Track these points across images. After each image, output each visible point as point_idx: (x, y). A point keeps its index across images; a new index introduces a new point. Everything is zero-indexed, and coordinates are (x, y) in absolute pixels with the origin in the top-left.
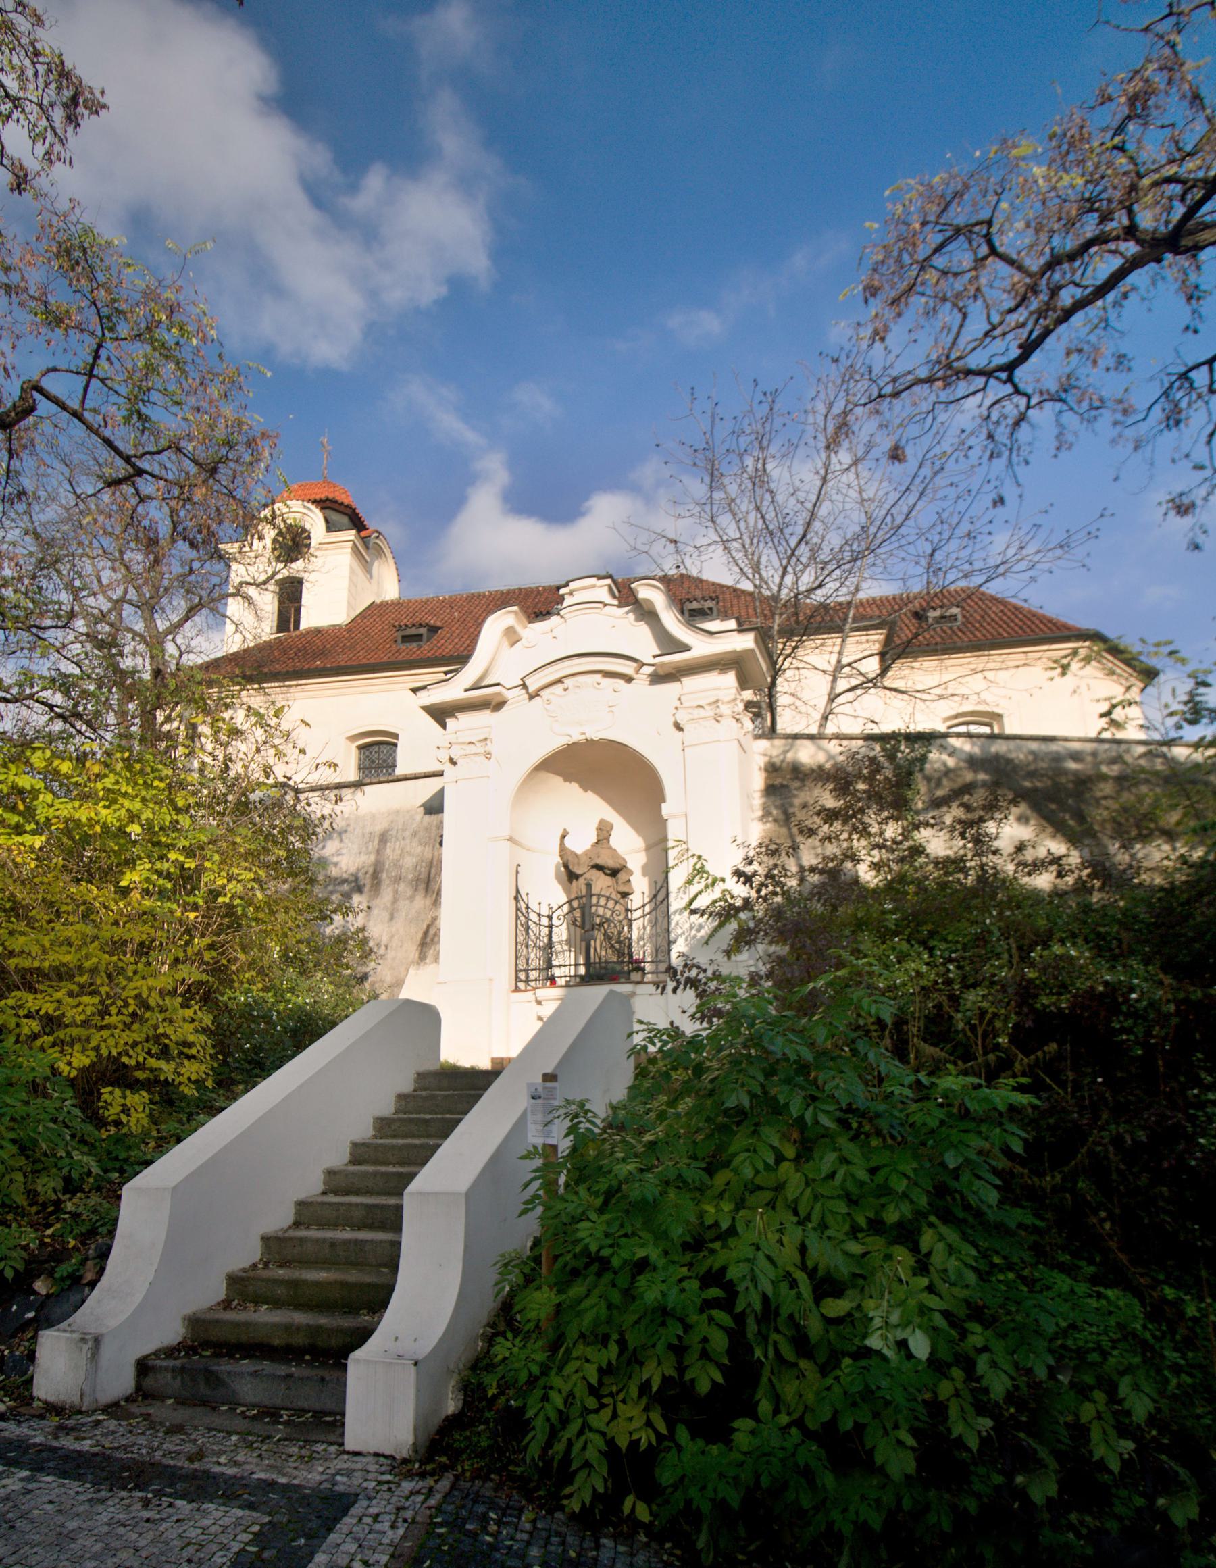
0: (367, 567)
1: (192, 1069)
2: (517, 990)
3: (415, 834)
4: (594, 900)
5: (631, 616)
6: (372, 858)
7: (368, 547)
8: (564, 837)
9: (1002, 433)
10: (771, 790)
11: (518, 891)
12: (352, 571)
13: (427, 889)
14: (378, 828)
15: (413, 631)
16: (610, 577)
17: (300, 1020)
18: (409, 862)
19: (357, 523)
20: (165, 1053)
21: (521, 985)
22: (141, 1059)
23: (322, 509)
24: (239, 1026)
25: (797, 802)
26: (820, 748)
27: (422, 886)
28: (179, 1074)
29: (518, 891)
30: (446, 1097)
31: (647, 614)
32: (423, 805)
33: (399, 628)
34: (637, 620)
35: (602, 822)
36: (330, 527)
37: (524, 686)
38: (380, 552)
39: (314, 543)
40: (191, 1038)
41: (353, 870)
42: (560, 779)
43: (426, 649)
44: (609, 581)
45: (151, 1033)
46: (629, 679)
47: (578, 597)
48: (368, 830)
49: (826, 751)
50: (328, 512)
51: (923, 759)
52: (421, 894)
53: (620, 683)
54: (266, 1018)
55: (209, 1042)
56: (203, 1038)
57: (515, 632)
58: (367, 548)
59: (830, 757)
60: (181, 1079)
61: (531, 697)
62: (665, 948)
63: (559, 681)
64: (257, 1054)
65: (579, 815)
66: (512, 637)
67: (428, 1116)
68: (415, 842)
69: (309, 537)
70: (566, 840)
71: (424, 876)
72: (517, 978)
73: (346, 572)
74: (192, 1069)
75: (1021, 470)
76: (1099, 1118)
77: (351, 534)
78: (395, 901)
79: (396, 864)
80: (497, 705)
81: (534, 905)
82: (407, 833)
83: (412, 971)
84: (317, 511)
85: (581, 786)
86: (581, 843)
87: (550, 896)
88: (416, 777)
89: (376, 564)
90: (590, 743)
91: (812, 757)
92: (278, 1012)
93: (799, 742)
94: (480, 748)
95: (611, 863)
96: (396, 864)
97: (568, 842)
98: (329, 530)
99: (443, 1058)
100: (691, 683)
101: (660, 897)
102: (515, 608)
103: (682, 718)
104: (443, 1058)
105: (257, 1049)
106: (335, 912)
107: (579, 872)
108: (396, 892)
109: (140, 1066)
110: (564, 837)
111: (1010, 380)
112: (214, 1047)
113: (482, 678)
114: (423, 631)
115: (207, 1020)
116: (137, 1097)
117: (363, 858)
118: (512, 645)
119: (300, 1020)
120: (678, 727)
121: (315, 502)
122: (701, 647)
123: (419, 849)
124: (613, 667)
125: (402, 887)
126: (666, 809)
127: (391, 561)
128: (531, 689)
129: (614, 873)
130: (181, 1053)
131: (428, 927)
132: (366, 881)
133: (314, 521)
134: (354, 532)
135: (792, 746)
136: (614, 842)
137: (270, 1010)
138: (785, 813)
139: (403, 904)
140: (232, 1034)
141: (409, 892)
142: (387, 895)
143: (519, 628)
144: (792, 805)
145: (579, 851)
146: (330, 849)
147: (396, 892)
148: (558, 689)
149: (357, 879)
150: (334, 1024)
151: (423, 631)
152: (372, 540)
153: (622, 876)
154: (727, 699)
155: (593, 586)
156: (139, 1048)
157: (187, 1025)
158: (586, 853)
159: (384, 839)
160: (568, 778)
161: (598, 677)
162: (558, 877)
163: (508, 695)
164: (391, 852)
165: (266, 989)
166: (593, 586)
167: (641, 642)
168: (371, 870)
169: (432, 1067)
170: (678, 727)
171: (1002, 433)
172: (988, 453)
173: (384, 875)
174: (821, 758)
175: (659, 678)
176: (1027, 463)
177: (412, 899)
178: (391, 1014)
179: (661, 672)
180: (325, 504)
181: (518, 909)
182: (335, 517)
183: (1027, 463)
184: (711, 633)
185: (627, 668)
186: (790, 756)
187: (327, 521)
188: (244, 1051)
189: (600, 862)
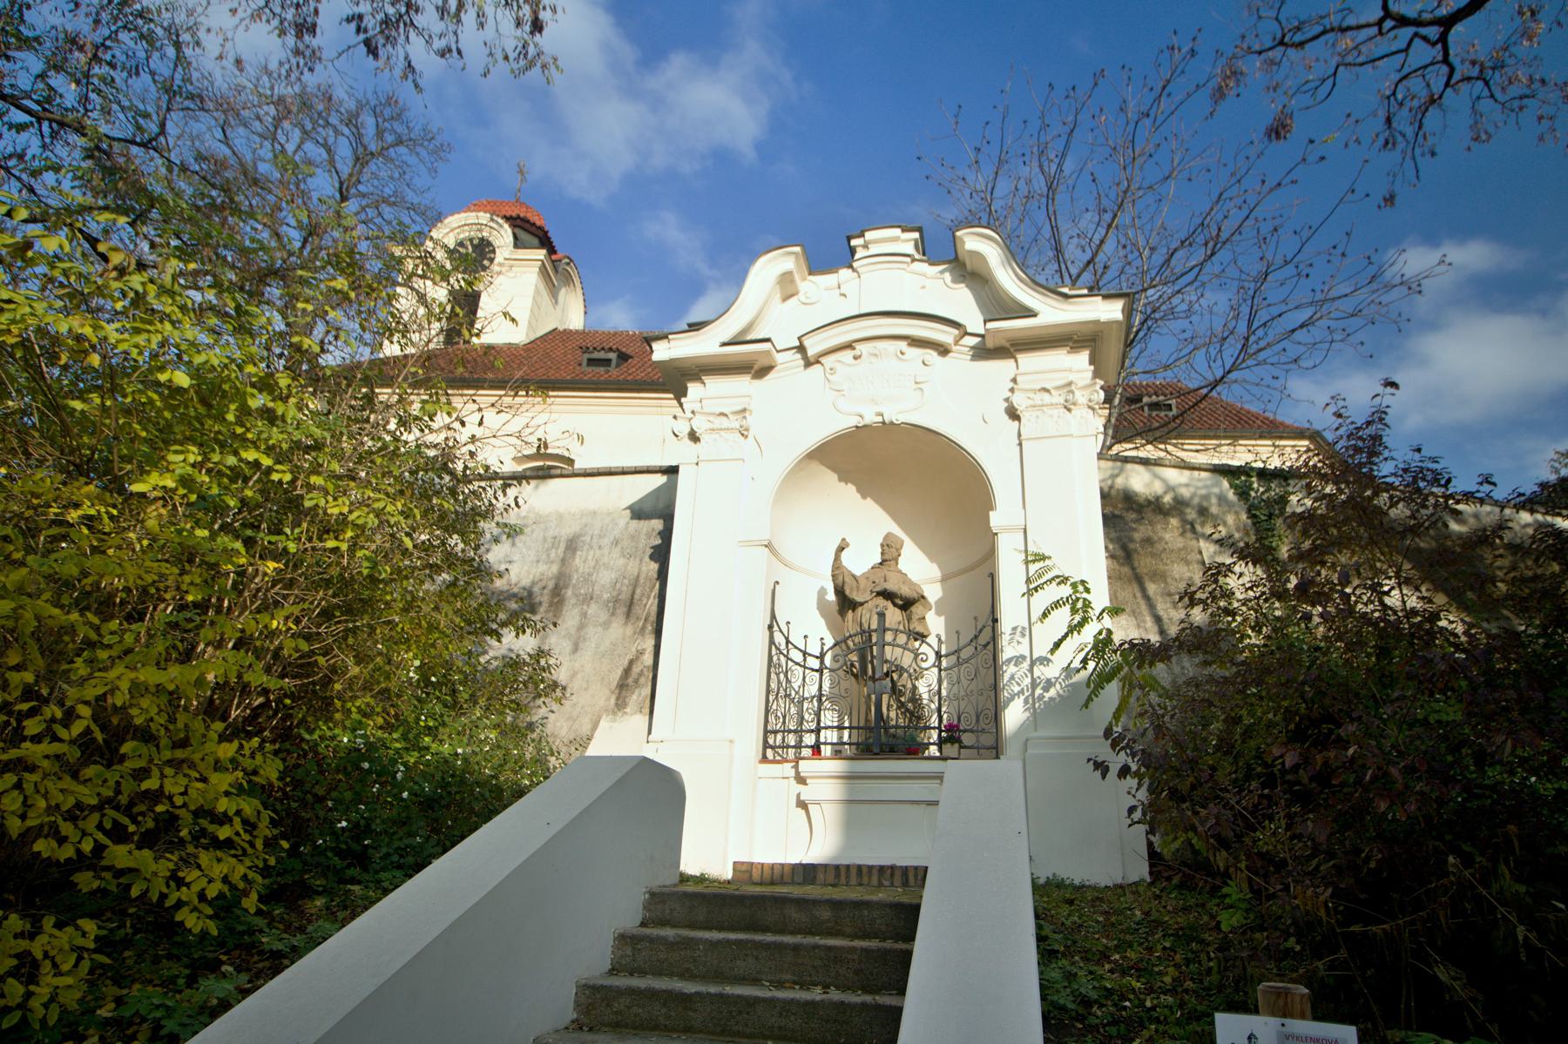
0: (554, 292)
1: (213, 872)
2: (764, 759)
3: (616, 542)
4: (889, 637)
5: (947, 276)
6: (555, 569)
7: (556, 273)
8: (841, 549)
9: (1403, 122)
10: (1109, 520)
11: (773, 617)
12: (537, 292)
13: (628, 614)
14: (567, 531)
15: (602, 355)
16: (919, 230)
17: (444, 785)
18: (605, 577)
19: (545, 242)
20: (161, 836)
21: (770, 753)
22: (87, 846)
23: (513, 226)
24: (333, 787)
25: (1137, 536)
26: (1156, 476)
27: (622, 610)
28: (180, 883)
29: (773, 617)
30: (714, 944)
31: (970, 273)
32: (630, 508)
33: (586, 350)
34: (954, 281)
35: (888, 536)
36: (518, 243)
37: (801, 349)
38: (568, 280)
39: (499, 258)
40: (223, 805)
41: (526, 582)
42: (835, 477)
43: (614, 372)
44: (916, 235)
45: (128, 787)
46: (943, 350)
47: (874, 250)
48: (551, 533)
49: (1164, 480)
50: (517, 231)
51: (1283, 500)
52: (620, 619)
53: (931, 355)
54: (385, 774)
55: (267, 814)
56: (249, 806)
57: (792, 281)
58: (556, 271)
59: (1170, 488)
60: (184, 893)
61: (808, 363)
62: (991, 714)
63: (849, 346)
64: (358, 838)
65: (857, 529)
66: (786, 280)
67: (690, 987)
68: (616, 552)
69: (494, 251)
70: (844, 555)
71: (625, 596)
72: (766, 745)
73: (531, 291)
74: (213, 872)
75: (1425, 163)
76: (1153, 934)
77: (541, 254)
78: (581, 627)
79: (587, 579)
80: (762, 371)
81: (797, 639)
82: (606, 541)
83: (604, 724)
84: (506, 226)
85: (859, 490)
86: (861, 561)
87: (812, 631)
88: (624, 472)
89: (563, 291)
90: (887, 427)
91: (1147, 485)
92: (405, 764)
93: (1129, 466)
94: (734, 423)
95: (905, 591)
96: (587, 579)
97: (846, 557)
98: (516, 246)
99: (691, 863)
100: (1028, 361)
101: (983, 639)
102: (797, 249)
103: (1019, 401)
104: (683, 868)
105: (360, 830)
106: (504, 624)
107: (859, 599)
108: (584, 615)
109: (93, 860)
110: (841, 549)
111: (1443, 39)
112: (273, 823)
113: (745, 331)
114: (612, 356)
115: (271, 771)
116: (66, 936)
117: (542, 568)
118: (786, 298)
119: (444, 785)
120: (1013, 414)
121: (508, 219)
122: (1051, 313)
123: (622, 561)
124: (924, 335)
125: (593, 609)
126: (996, 519)
127: (580, 292)
128: (811, 352)
129: (906, 604)
130: (199, 836)
131: (631, 662)
132: (544, 599)
133: (503, 237)
134: (544, 252)
135: (1122, 470)
136: (903, 564)
137: (394, 762)
138: (1124, 548)
139: (593, 633)
140: (321, 800)
141: (604, 616)
142: (570, 618)
143: (797, 277)
144: (1132, 540)
145: (858, 573)
146: (495, 556)
147: (584, 615)
148: (847, 356)
149: (530, 594)
150: (520, 793)
151: (612, 356)
152: (562, 266)
153: (917, 610)
154: (1081, 384)
155: (896, 239)
156: (91, 823)
157: (220, 777)
158: (866, 576)
159: (572, 546)
160: (844, 477)
161: (903, 345)
162: (822, 605)
163: (779, 358)
164: (581, 563)
165: (387, 727)
166: (896, 239)
167: (961, 304)
168: (551, 585)
169: (666, 880)
170: (1013, 414)
171: (1403, 122)
172: (1381, 141)
173: (569, 592)
174: (1158, 488)
175: (985, 352)
176: (1433, 154)
177: (606, 625)
178: (620, 782)
179: (990, 344)
180: (518, 223)
181: (772, 642)
182: (523, 235)
183: (1433, 154)
184: (1066, 296)
185: (945, 335)
186: (1120, 481)
187: (515, 237)
188: (335, 833)
189: (891, 586)
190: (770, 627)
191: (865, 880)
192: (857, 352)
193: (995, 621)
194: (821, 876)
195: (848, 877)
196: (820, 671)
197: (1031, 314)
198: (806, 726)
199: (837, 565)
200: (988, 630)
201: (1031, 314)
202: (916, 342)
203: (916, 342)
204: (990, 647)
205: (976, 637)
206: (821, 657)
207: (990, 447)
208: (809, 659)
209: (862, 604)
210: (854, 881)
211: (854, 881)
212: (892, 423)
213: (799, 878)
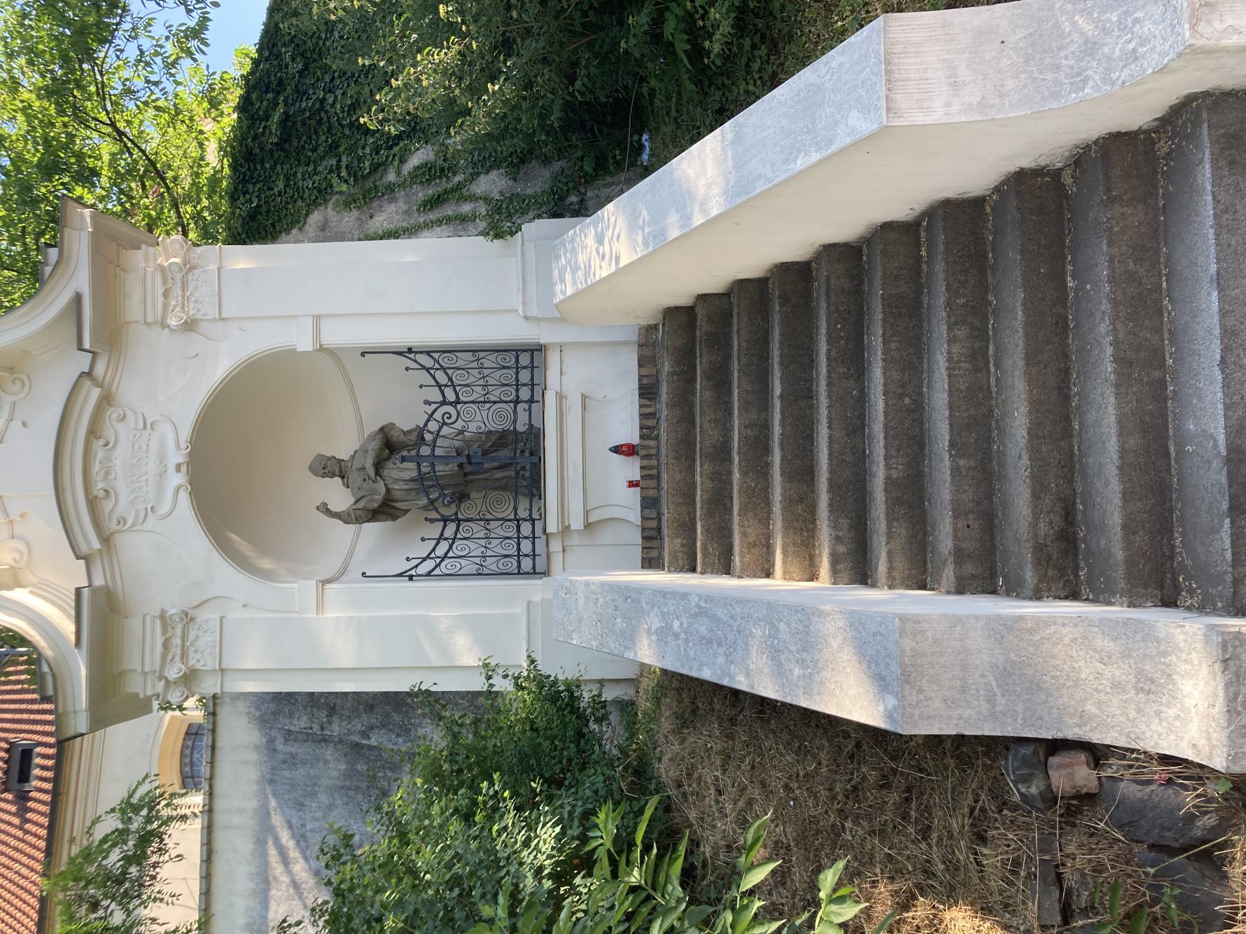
63: (92, 503)
95: (374, 445)
101: (428, 362)
136: (344, 454)
153: (395, 436)
163: (99, 581)
189: (369, 462)
190: (411, 578)
191: (653, 451)
192: (101, 494)
193: (410, 350)
194: (651, 493)
195: (650, 468)
196: (459, 522)
197: (78, 298)
198: (513, 551)
199: (345, 517)
200: (419, 358)
201: (78, 298)
202: (94, 432)
203: (94, 432)
204: (436, 355)
205: (428, 370)
206: (445, 520)
207: (221, 361)
208: (446, 535)
209: (388, 490)
210: (654, 462)
211: (654, 462)
212: (190, 454)
213: (653, 514)
